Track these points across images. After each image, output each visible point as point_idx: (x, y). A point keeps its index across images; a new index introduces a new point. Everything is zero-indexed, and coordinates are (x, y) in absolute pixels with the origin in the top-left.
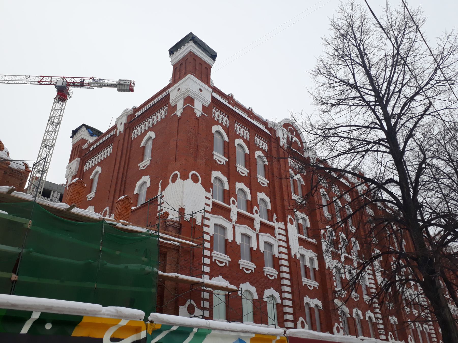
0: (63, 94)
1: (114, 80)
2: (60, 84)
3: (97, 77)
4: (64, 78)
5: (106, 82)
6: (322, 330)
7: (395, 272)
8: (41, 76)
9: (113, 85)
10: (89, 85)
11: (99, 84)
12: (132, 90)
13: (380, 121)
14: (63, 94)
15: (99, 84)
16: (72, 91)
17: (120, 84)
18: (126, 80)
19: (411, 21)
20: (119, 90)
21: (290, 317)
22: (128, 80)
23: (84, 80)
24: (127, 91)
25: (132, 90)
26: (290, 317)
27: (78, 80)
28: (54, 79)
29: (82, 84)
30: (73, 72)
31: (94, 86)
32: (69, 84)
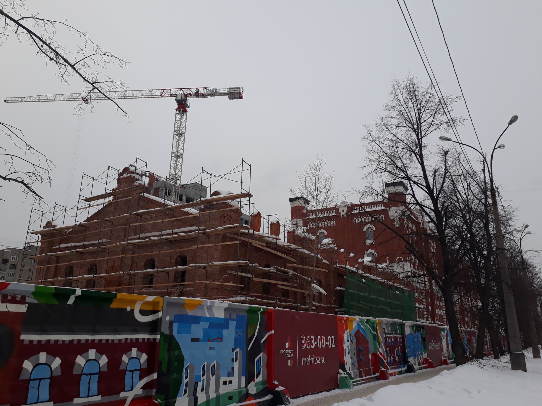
0: (182, 106)
1: (225, 89)
2: (179, 97)
3: (210, 87)
4: (181, 89)
5: (218, 91)
6: (154, 195)
7: (478, 256)
8: (162, 89)
9: (225, 94)
10: (203, 95)
11: (213, 93)
12: (242, 98)
13: (176, 286)
14: (182, 106)
15: (213, 93)
16: (191, 101)
17: (231, 93)
18: (235, 88)
19: (412, 83)
20: (230, 98)
21: (426, 316)
22: (237, 88)
23: (198, 90)
24: (237, 98)
25: (242, 98)
26: (426, 316)
27: (194, 91)
28: (173, 92)
29: (197, 95)
30: (190, 84)
31: (208, 95)
32: (186, 96)
